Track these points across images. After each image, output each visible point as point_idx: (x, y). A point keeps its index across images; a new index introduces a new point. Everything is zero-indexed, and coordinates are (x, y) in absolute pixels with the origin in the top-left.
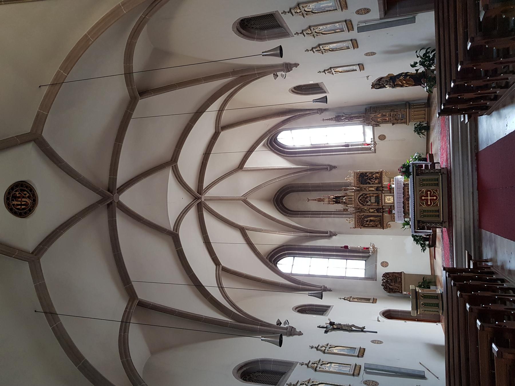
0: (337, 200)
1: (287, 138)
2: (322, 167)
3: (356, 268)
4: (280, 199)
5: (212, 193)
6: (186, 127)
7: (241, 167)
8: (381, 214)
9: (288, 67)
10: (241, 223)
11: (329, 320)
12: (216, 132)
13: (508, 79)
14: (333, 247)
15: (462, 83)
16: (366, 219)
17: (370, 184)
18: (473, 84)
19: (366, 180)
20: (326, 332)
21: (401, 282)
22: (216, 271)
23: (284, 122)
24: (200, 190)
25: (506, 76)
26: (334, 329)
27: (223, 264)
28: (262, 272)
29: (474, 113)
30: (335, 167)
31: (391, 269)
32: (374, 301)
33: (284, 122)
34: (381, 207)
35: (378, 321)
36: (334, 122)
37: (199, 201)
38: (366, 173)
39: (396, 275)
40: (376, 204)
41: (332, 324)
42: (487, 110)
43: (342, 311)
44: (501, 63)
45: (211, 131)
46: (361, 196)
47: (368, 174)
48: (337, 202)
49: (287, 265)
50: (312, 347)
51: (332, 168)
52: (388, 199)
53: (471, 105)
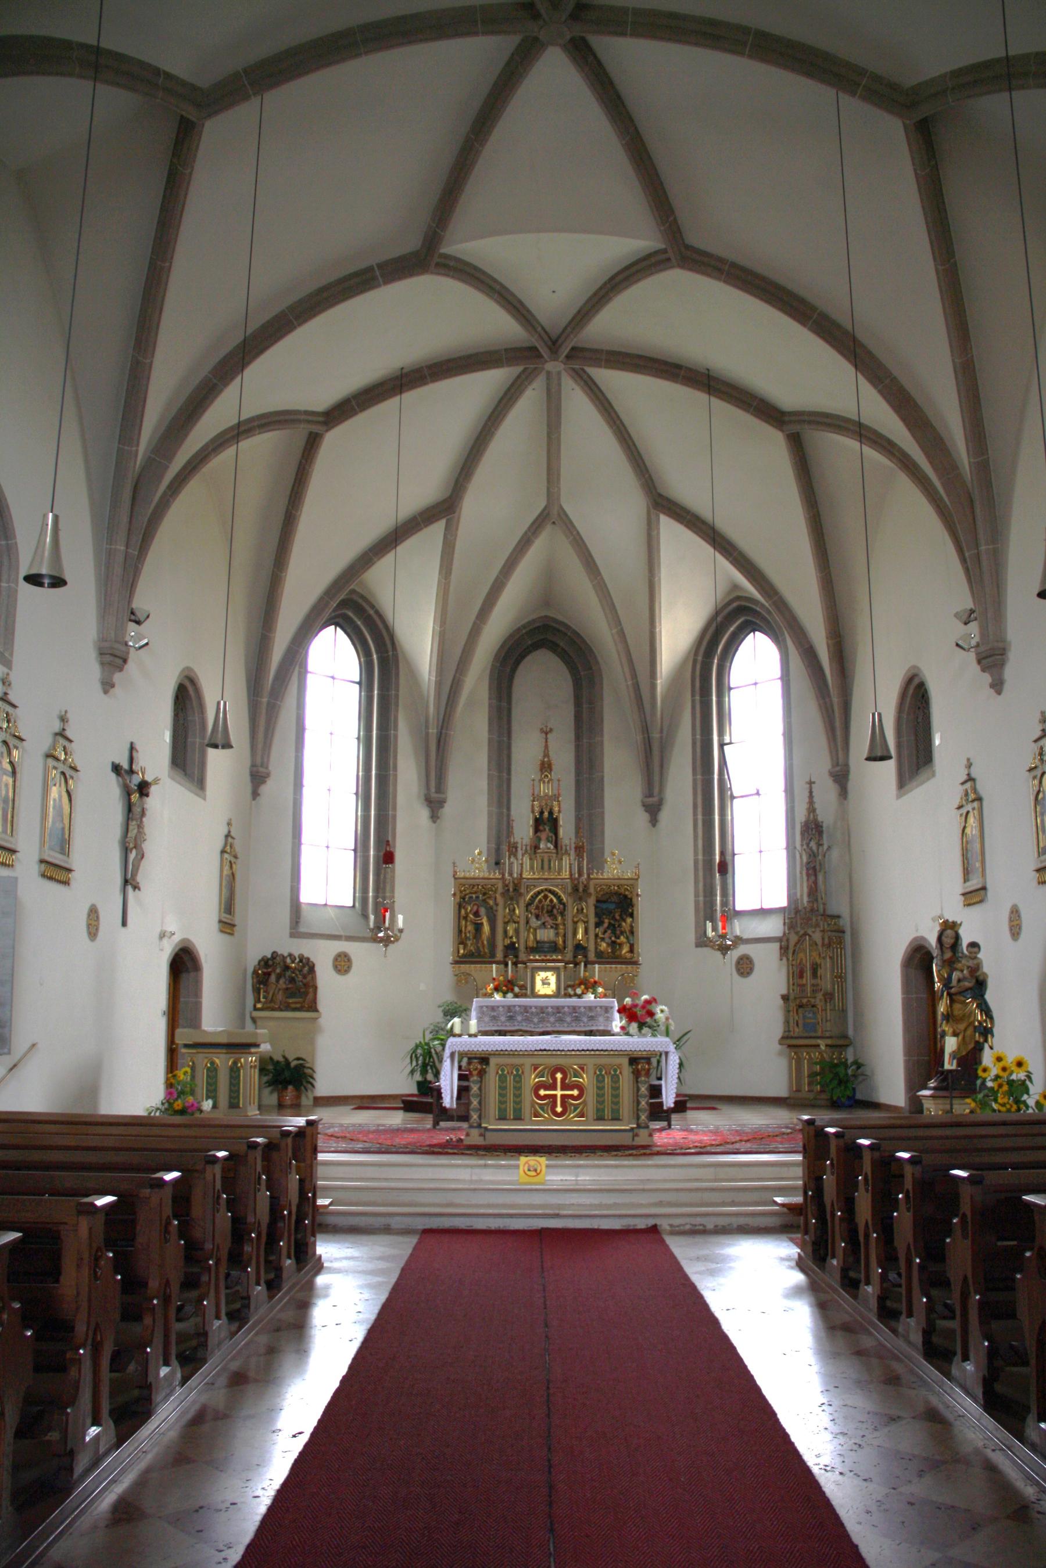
0: (546, 823)
1: (757, 664)
2: (656, 778)
3: (328, 874)
4: (547, 636)
5: (577, 404)
6: (802, 301)
7: (662, 503)
8: (499, 955)
9: (992, 658)
10: (470, 506)
11: (156, 781)
12: (783, 413)
13: (910, 1315)
14: (395, 809)
15: (908, 1184)
16: (482, 911)
17: (598, 925)
18: (903, 1218)
19: (610, 913)
20: (116, 768)
21: (288, 1008)
22: (306, 413)
23: (809, 654)
24: (583, 359)
25: (920, 1312)
26: (127, 792)
27: (333, 439)
28: (308, 577)
29: (807, 1223)
30: (654, 821)
31: (325, 977)
32: (227, 926)
33: (809, 654)
34: (522, 956)
35: (162, 936)
36: (801, 816)
37: (544, 351)
38: (631, 915)
39: (311, 996)
40: (531, 944)
41: (143, 788)
42: (814, 1258)
43: (185, 825)
44: (965, 1297)
45: (787, 396)
46: (559, 898)
47: (629, 920)
48: (538, 823)
49: (333, 661)
50: (63, 719)
51: (653, 810)
52: (546, 982)
53: (833, 1215)
